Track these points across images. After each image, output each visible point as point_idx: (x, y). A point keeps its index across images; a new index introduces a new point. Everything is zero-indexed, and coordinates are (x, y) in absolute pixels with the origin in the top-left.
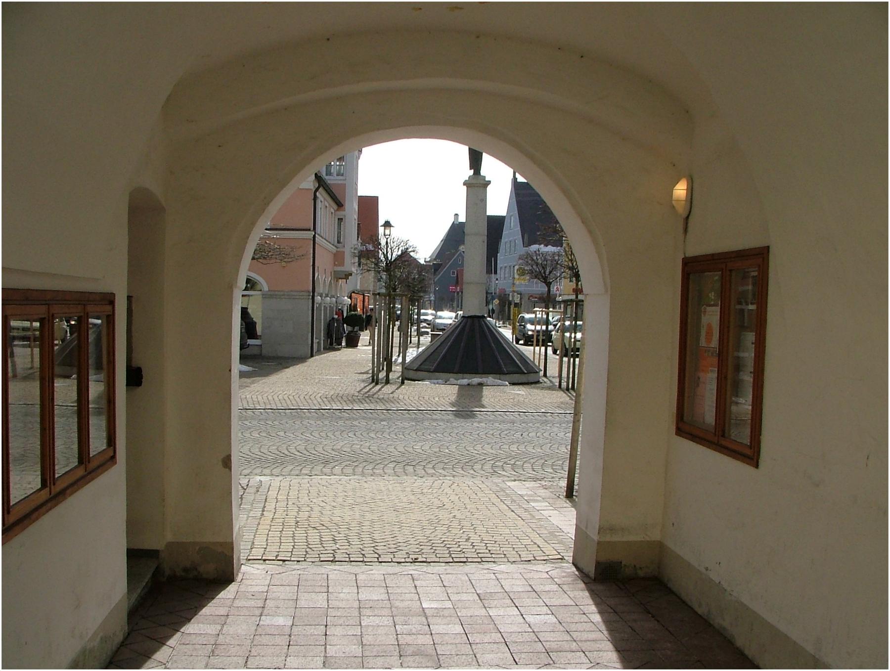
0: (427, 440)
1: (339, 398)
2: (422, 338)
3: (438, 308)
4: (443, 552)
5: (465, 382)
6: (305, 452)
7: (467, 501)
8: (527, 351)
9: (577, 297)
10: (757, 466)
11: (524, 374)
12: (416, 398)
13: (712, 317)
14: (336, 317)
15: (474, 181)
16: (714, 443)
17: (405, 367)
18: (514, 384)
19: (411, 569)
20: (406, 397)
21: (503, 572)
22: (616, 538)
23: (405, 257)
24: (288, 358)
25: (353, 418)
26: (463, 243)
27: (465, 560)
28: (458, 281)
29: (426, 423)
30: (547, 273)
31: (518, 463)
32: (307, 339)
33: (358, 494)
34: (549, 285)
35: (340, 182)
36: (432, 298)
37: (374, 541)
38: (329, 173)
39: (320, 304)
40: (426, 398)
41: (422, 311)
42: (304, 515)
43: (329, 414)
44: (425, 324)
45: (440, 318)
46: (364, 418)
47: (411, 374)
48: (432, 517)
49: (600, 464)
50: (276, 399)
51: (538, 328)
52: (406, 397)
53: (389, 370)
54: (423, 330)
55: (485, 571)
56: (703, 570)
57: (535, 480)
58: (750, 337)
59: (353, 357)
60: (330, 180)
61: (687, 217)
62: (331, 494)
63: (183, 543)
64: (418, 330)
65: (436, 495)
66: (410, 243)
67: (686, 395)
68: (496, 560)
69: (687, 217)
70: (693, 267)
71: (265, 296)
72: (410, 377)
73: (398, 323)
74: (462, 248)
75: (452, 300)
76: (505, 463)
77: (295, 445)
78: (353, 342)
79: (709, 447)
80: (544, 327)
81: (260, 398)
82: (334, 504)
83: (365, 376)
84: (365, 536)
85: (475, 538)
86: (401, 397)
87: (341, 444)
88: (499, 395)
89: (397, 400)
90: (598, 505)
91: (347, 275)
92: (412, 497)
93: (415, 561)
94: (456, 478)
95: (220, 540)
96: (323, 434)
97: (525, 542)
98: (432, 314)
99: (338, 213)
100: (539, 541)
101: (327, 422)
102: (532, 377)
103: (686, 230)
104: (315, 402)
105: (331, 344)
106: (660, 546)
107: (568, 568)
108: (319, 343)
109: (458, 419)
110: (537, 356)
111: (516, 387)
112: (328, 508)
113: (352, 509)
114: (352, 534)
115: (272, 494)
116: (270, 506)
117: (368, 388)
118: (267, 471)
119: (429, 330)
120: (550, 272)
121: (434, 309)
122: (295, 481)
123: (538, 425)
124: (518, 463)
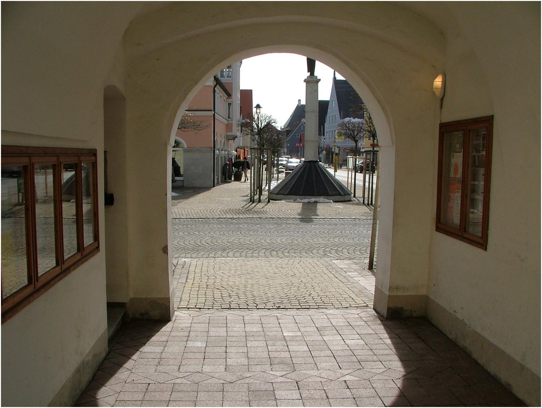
1: (231, 211)
2: (280, 175)
5: (306, 200)
7: (309, 272)
9: (373, 149)
10: (486, 249)
12: (277, 211)
13: (457, 159)
14: (228, 162)
15: (311, 80)
16: (458, 236)
19: (276, 313)
22: (400, 293)
23: (269, 126)
24: (200, 188)
25: (239, 223)
26: (304, 117)
27: (308, 307)
28: (301, 140)
30: (356, 133)
34: (356, 142)
37: (254, 296)
38: (222, 76)
39: (218, 155)
40: (283, 210)
41: (280, 159)
42: (211, 281)
44: (281, 167)
45: (291, 162)
46: (246, 223)
47: (274, 196)
48: (288, 282)
50: (193, 212)
52: (271, 210)
53: (261, 194)
55: (321, 314)
56: (453, 313)
57: (350, 259)
58: (482, 171)
59: (238, 187)
60: (223, 80)
61: (442, 99)
62: (227, 268)
64: (277, 170)
65: (290, 268)
66: (272, 118)
69: (442, 99)
71: (185, 151)
74: (303, 120)
75: (298, 152)
76: (331, 249)
81: (183, 212)
83: (246, 198)
85: (314, 294)
86: (268, 210)
88: (327, 208)
90: (389, 273)
91: (234, 138)
92: (276, 270)
93: (279, 308)
94: (302, 258)
97: (346, 296)
98: (286, 161)
100: (353, 296)
101: (224, 226)
102: (347, 198)
103: (441, 107)
104: (216, 214)
105: (225, 179)
106: (426, 299)
108: (218, 179)
110: (349, 185)
111: (337, 204)
112: (226, 277)
113: (240, 277)
114: (241, 292)
115: (192, 269)
116: (191, 276)
117: (248, 205)
118: (188, 255)
119: (284, 170)
120: (357, 134)
122: (206, 261)
124: (339, 249)
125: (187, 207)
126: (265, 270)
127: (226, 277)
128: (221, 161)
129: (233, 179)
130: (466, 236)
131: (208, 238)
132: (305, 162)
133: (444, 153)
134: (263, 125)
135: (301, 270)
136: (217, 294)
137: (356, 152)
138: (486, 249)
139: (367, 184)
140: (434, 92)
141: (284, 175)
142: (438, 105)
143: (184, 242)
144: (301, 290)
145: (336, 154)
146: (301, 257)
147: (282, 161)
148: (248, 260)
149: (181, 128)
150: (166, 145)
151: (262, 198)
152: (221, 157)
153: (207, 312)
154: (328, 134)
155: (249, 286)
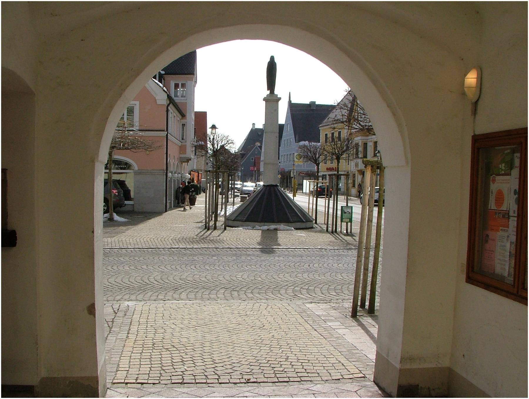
3: (244, 180)
4: (269, 372)
5: (266, 228)
7: (280, 322)
9: (338, 173)
12: (235, 239)
14: (181, 186)
18: (297, 229)
20: (228, 239)
22: (415, 366)
25: (194, 255)
27: (287, 379)
28: (256, 163)
29: (243, 258)
34: (318, 165)
35: (182, 101)
36: (240, 175)
38: (176, 96)
39: (171, 178)
40: (242, 239)
41: (236, 182)
42: (159, 336)
43: (178, 252)
45: (246, 186)
46: (201, 254)
47: (231, 223)
48: (256, 337)
50: (142, 241)
52: (228, 239)
53: (216, 220)
55: (306, 392)
60: (177, 100)
61: (476, 102)
62: (180, 317)
63: (54, 378)
65: (256, 317)
66: (229, 138)
68: (312, 379)
69: (476, 102)
72: (230, 225)
75: (252, 176)
77: (153, 276)
78: (192, 202)
81: (131, 240)
82: (182, 326)
83: (200, 225)
85: (292, 358)
86: (225, 239)
87: (186, 274)
88: (288, 237)
89: (222, 241)
90: (400, 339)
91: (188, 160)
92: (240, 319)
93: (248, 382)
94: (269, 301)
96: (173, 267)
97: (333, 360)
99: (182, 120)
100: (343, 360)
101: (176, 258)
102: (308, 225)
104: (168, 243)
105: (178, 203)
107: (372, 387)
108: (171, 203)
111: (299, 231)
113: (195, 331)
115: (136, 317)
116: (134, 329)
117: (203, 233)
118: (133, 297)
119: (239, 194)
122: (154, 305)
125: (135, 235)
126: (226, 319)
128: (174, 184)
131: (157, 274)
134: (219, 146)
135: (270, 319)
136: (167, 361)
137: (312, 176)
139: (331, 211)
141: (240, 200)
144: (275, 351)
146: (267, 299)
148: (204, 304)
150: (93, 161)
151: (218, 224)
152: (174, 181)
153: (152, 390)
154: (283, 158)
155: (207, 344)
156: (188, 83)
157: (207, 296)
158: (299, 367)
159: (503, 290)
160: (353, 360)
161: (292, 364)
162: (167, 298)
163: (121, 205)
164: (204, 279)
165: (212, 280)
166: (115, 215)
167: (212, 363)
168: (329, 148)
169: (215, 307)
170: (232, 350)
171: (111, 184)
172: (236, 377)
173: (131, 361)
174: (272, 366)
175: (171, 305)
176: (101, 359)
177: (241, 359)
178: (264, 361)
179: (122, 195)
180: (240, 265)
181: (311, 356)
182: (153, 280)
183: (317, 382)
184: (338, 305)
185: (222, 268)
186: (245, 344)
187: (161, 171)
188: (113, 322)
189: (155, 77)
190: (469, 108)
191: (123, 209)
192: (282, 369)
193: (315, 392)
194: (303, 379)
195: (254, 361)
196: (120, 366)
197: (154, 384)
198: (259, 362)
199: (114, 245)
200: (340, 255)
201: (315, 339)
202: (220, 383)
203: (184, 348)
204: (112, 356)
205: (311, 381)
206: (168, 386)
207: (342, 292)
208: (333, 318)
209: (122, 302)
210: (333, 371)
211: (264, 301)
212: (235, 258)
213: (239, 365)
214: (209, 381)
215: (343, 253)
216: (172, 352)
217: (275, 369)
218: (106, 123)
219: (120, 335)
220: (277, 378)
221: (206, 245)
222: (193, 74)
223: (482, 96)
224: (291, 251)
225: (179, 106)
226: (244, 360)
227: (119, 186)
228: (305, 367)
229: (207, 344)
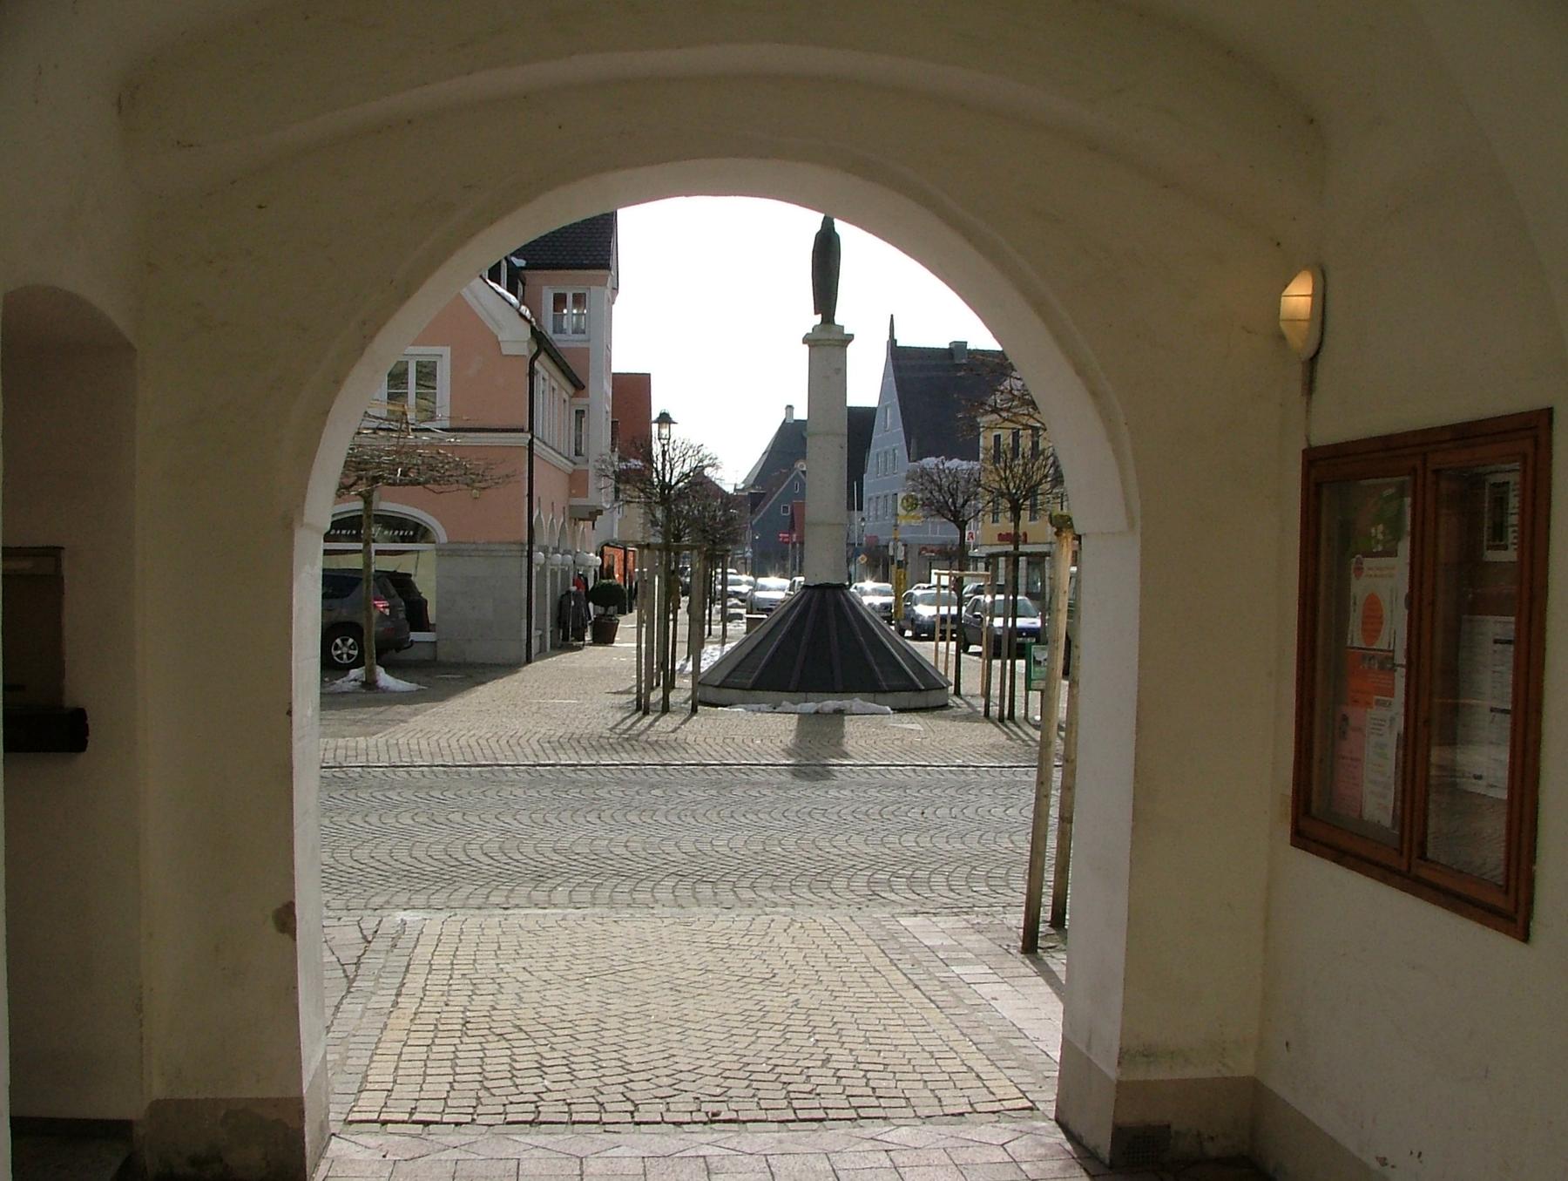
0: (740, 827)
1: (575, 741)
2: (730, 626)
3: (759, 571)
4: (773, 1094)
5: (810, 707)
6: (499, 856)
7: (821, 964)
8: (925, 649)
9: (1016, 548)
10: (1525, 936)
11: (919, 692)
12: (720, 740)
13: (1384, 581)
14: (574, 589)
15: (824, 336)
16: (1398, 873)
17: (699, 681)
18: (901, 711)
19: (705, 1141)
20: (700, 739)
21: (907, 1147)
22: (1159, 1073)
23: (699, 482)
24: (483, 665)
25: (598, 783)
26: (803, 456)
27: (820, 1114)
28: (794, 523)
29: (738, 791)
30: (960, 501)
31: (918, 874)
32: (520, 631)
33: (599, 952)
34: (962, 526)
37: (626, 1067)
38: (559, 329)
39: (543, 567)
40: (738, 739)
42: (482, 1003)
43: (555, 776)
44: (735, 601)
45: (763, 588)
46: (619, 782)
47: (711, 694)
48: (749, 1005)
49: (1122, 913)
50: (454, 744)
51: (944, 610)
52: (700, 739)
53: (669, 686)
54: (732, 611)
55: (868, 1145)
56: (1375, 1165)
57: (955, 911)
58: (1498, 626)
59: (604, 662)
60: (560, 341)
62: (544, 951)
64: (723, 611)
65: (757, 951)
66: (705, 451)
67: (1316, 756)
70: (1332, 474)
71: (442, 552)
73: (685, 600)
74: (801, 465)
75: (784, 558)
76: (894, 874)
78: (605, 635)
79: (1470, 916)
80: (954, 610)
81: (423, 742)
82: (547, 975)
83: (625, 699)
84: (606, 1054)
85: (841, 1058)
86: (691, 738)
88: (876, 733)
89: (682, 746)
90: (1117, 999)
91: (593, 514)
92: (709, 957)
93: (714, 1119)
95: (274, 1093)
96: (538, 817)
97: (954, 1065)
98: (749, 583)
100: (981, 1065)
101: (547, 792)
102: (933, 698)
103: (1309, 387)
104: (528, 751)
105: (565, 638)
106: (1255, 1093)
107: (1049, 1134)
108: (542, 637)
109: (798, 782)
110: (942, 657)
111: (906, 717)
112: (535, 984)
113: (583, 988)
114: (581, 1049)
116: (415, 983)
117: (629, 722)
118: (420, 899)
119: (743, 611)
120: (966, 502)
121: (752, 574)
122: (474, 920)
123: (951, 792)
124: (918, 874)
125: (436, 728)
126: (672, 958)
127: (535, 984)
129: (588, 638)
130: (1424, 873)
132: (805, 587)
133: (1322, 558)
135: (794, 957)
138: (1525, 936)
140: (1281, 337)
141: (744, 627)
142: (1297, 387)
143: (410, 850)
145: (900, 564)
146: (792, 906)
147: (738, 583)
148: (614, 916)
149: (427, 482)
150: (288, 524)
152: (554, 574)
153: (453, 1140)
154: (873, 505)
155: (613, 1023)
156: (593, 293)
157: (626, 897)
158: (856, 1082)
159: (1377, 864)
160: (1009, 1063)
161: (840, 1074)
162: (513, 902)
163: (402, 645)
164: (620, 850)
165: (643, 854)
166: (381, 672)
167: (620, 1071)
168: (992, 479)
169: (645, 925)
170: (679, 1037)
171: (368, 581)
172: (681, 1108)
173: (402, 1064)
174: (784, 1078)
175: (523, 923)
176: (314, 1053)
177: (700, 1063)
178: (764, 1067)
179: (402, 615)
180: (726, 813)
181: (895, 1054)
182: (477, 854)
183: (902, 1122)
184: (990, 919)
185: (674, 819)
186: (717, 1021)
187: (515, 547)
188: (357, 964)
189: (494, 274)
190: (1297, 372)
191: (404, 655)
192: (808, 1087)
193: (890, 1147)
194: (862, 1113)
195: (737, 1066)
196: (370, 1079)
197: (457, 1124)
198: (750, 1068)
199: (373, 756)
200: (1014, 784)
201: (911, 1010)
202: (638, 1124)
203: (548, 1034)
204: (350, 1053)
205: (885, 1118)
206: (496, 1129)
207: (1008, 885)
208: (969, 955)
209: (386, 913)
210: (947, 1093)
211: (783, 910)
212: (714, 792)
213: (693, 1077)
214: (605, 1118)
215: (1025, 778)
216: (515, 1044)
217: (790, 1088)
218: (324, 424)
219: (374, 998)
220: (795, 1110)
221: (634, 756)
222: (607, 267)
223: (1326, 339)
224: (878, 772)
225: (565, 360)
226: (709, 1063)
227: (393, 591)
228: (872, 1083)
229: (613, 1023)
